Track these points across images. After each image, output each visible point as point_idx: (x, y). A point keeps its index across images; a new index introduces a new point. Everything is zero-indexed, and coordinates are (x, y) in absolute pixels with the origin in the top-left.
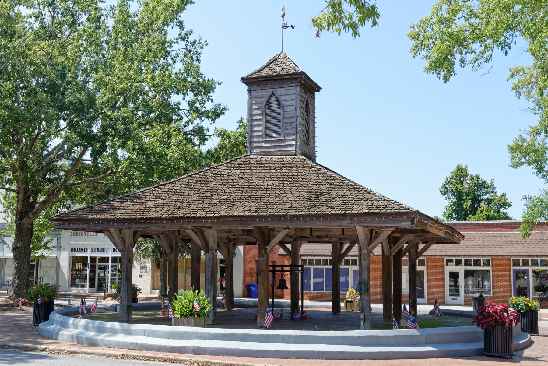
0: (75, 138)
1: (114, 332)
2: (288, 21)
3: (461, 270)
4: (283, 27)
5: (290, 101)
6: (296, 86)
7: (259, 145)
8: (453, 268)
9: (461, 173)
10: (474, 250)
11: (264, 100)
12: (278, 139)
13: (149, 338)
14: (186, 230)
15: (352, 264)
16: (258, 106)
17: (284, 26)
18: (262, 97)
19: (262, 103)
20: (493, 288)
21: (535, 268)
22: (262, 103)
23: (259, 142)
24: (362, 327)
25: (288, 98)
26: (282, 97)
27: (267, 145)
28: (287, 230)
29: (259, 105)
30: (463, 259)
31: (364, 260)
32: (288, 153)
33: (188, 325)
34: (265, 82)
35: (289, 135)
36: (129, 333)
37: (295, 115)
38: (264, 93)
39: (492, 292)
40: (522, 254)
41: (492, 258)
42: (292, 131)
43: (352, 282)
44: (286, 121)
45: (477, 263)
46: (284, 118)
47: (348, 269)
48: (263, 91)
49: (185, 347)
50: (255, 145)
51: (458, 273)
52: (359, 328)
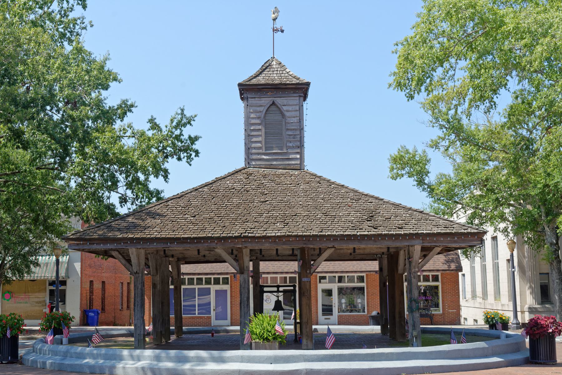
0: (50, 142)
1: (201, 360)
2: (278, 25)
4: (273, 31)
5: (293, 112)
6: (300, 96)
7: (259, 157)
10: (352, 266)
11: (263, 109)
12: (279, 151)
14: (216, 250)
15: (214, 284)
16: (256, 115)
17: (275, 30)
18: (261, 106)
19: (260, 112)
20: (368, 306)
22: (260, 112)
23: (258, 154)
24: (415, 343)
25: (290, 108)
26: (283, 107)
27: (267, 157)
28: (333, 249)
29: (258, 114)
30: (337, 275)
31: (414, 278)
32: (292, 167)
33: (271, 348)
34: (265, 90)
35: (293, 147)
36: (222, 360)
37: (299, 127)
38: (263, 102)
39: (366, 310)
41: (367, 274)
42: (295, 144)
43: (214, 304)
44: (290, 133)
45: (351, 280)
46: (288, 129)
47: (210, 289)
48: (262, 99)
50: (254, 157)
52: (413, 346)
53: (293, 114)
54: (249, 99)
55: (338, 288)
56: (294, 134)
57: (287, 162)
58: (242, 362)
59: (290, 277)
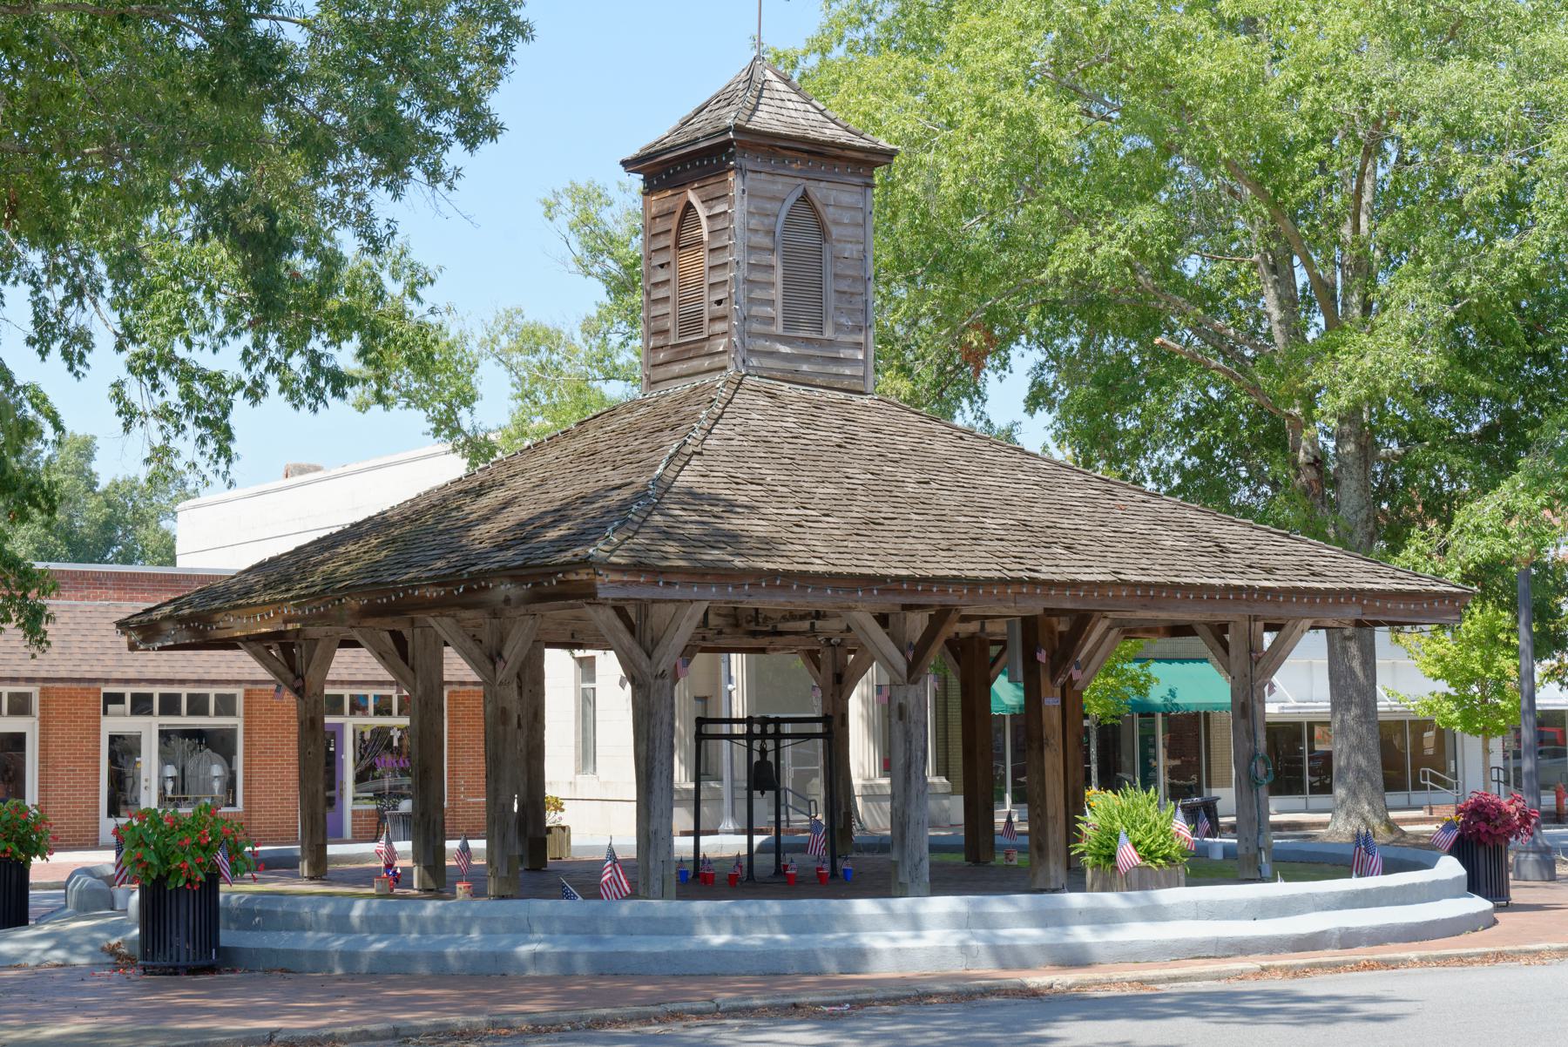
3: (148, 728)
7: (767, 345)
8: (119, 722)
9: (253, 404)
13: (1211, 922)
14: (854, 614)
16: (763, 224)
21: (359, 720)
32: (846, 384)
40: (360, 677)
45: (198, 705)
49: (1324, 932)
51: (138, 738)
53: (849, 231)
54: (749, 175)
55: (161, 732)
56: (852, 290)
57: (834, 369)
58: (1197, 918)
59: (162, 696)
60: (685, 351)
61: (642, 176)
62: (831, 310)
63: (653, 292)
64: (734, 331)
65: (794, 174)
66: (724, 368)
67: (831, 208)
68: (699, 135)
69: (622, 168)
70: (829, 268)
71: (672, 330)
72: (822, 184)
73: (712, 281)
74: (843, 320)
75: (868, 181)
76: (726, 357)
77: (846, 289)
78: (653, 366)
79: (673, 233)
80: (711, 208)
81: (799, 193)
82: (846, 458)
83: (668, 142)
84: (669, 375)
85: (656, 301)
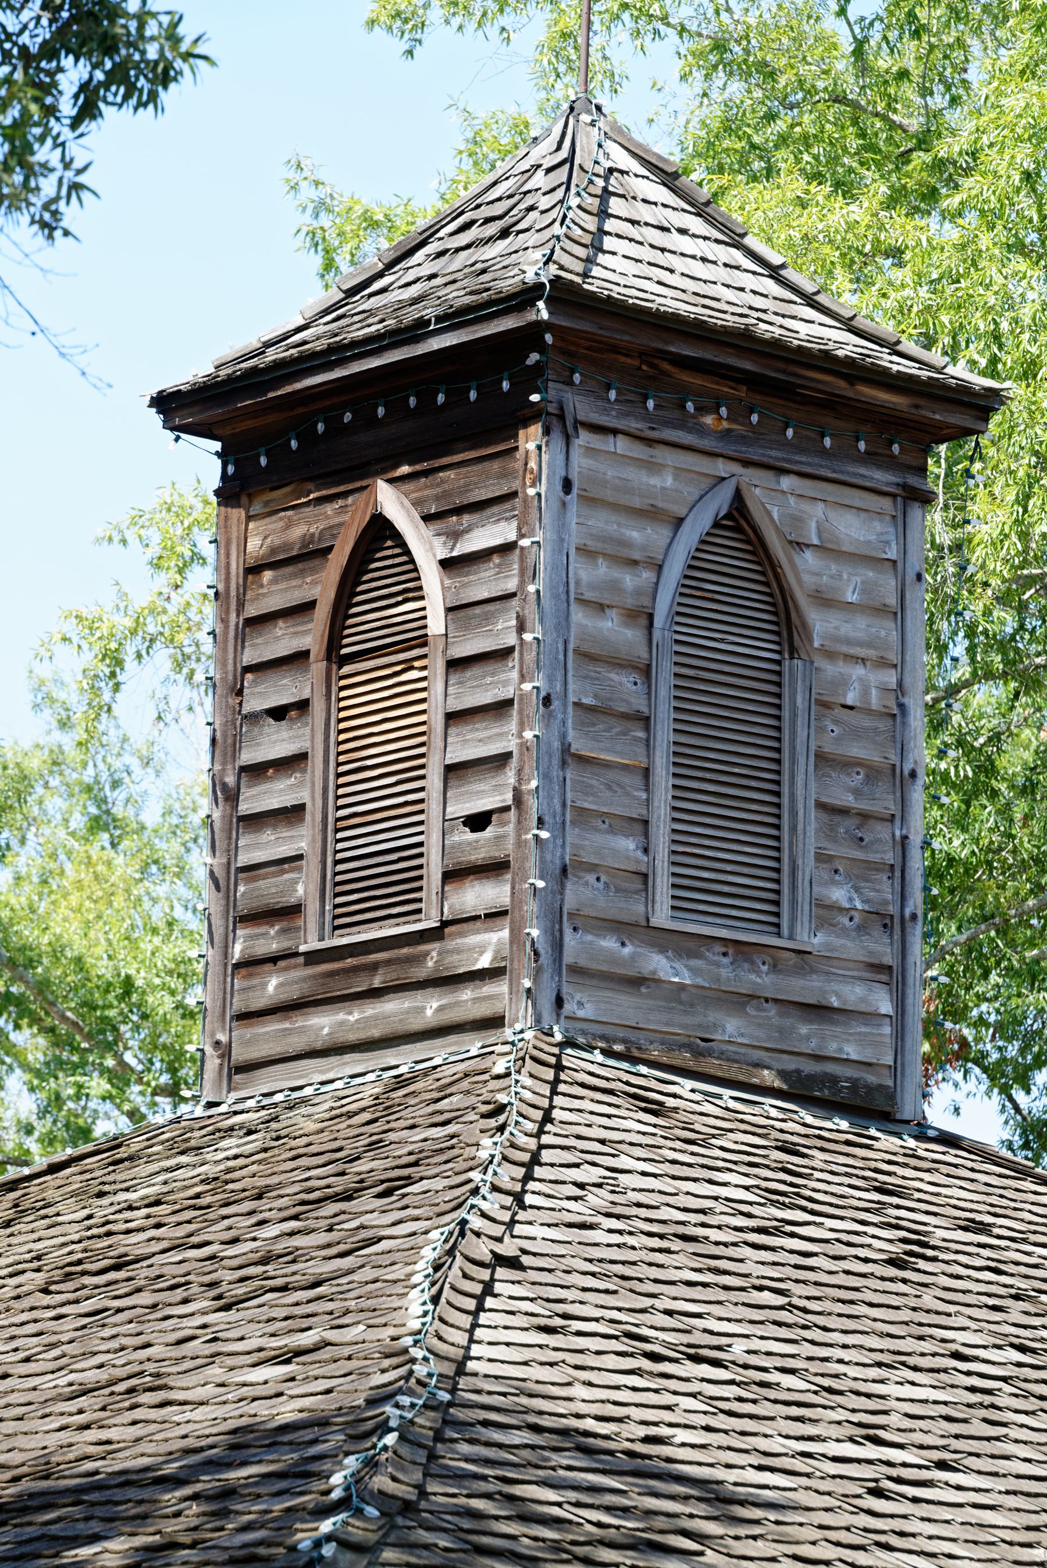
53: (858, 627)
54: (584, 438)
56: (864, 806)
60: (355, 970)
61: (217, 446)
62: (808, 865)
63: (246, 793)
64: (531, 907)
65: (706, 443)
66: (495, 1022)
67: (808, 555)
68: (429, 311)
69: (155, 419)
70: (802, 733)
71: (312, 909)
72: (787, 482)
73: (452, 758)
74: (839, 894)
75: (913, 480)
76: (502, 987)
77: (848, 800)
78: (245, 1017)
79: (322, 612)
80: (455, 536)
81: (720, 501)
82: (928, 1300)
83: (317, 336)
84: (297, 1044)
85: (256, 821)
